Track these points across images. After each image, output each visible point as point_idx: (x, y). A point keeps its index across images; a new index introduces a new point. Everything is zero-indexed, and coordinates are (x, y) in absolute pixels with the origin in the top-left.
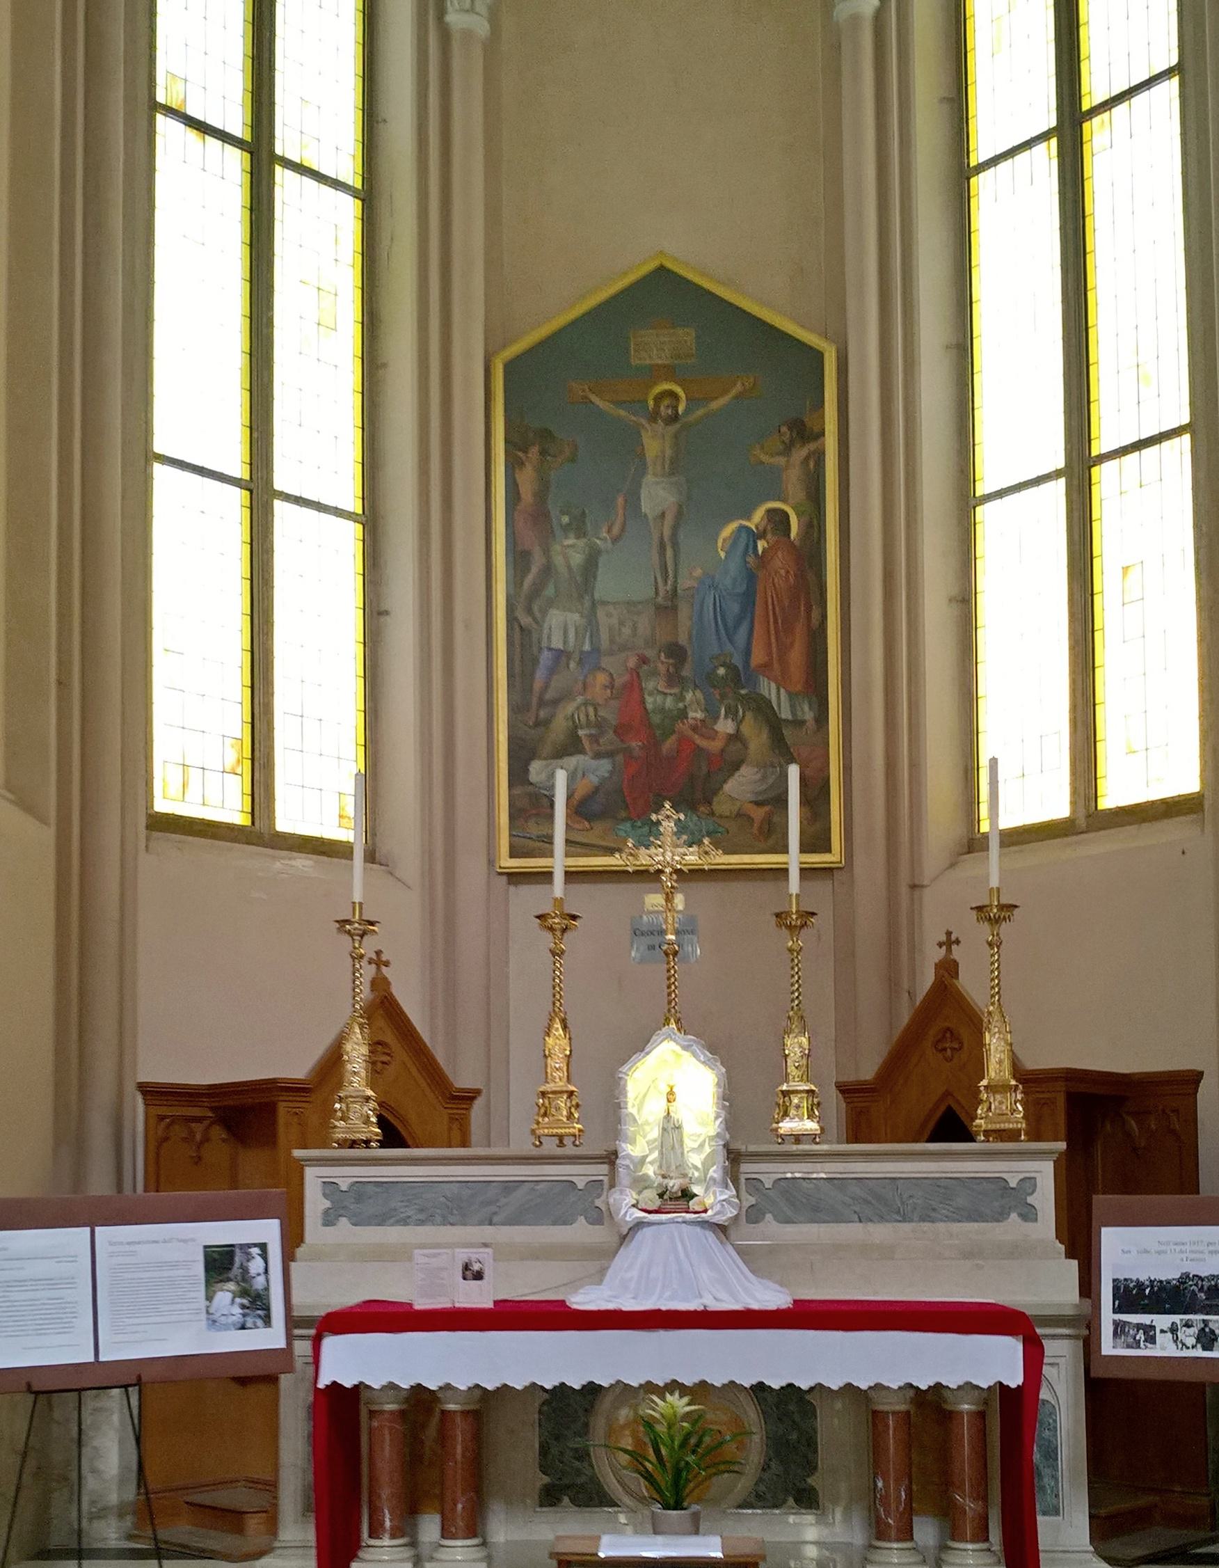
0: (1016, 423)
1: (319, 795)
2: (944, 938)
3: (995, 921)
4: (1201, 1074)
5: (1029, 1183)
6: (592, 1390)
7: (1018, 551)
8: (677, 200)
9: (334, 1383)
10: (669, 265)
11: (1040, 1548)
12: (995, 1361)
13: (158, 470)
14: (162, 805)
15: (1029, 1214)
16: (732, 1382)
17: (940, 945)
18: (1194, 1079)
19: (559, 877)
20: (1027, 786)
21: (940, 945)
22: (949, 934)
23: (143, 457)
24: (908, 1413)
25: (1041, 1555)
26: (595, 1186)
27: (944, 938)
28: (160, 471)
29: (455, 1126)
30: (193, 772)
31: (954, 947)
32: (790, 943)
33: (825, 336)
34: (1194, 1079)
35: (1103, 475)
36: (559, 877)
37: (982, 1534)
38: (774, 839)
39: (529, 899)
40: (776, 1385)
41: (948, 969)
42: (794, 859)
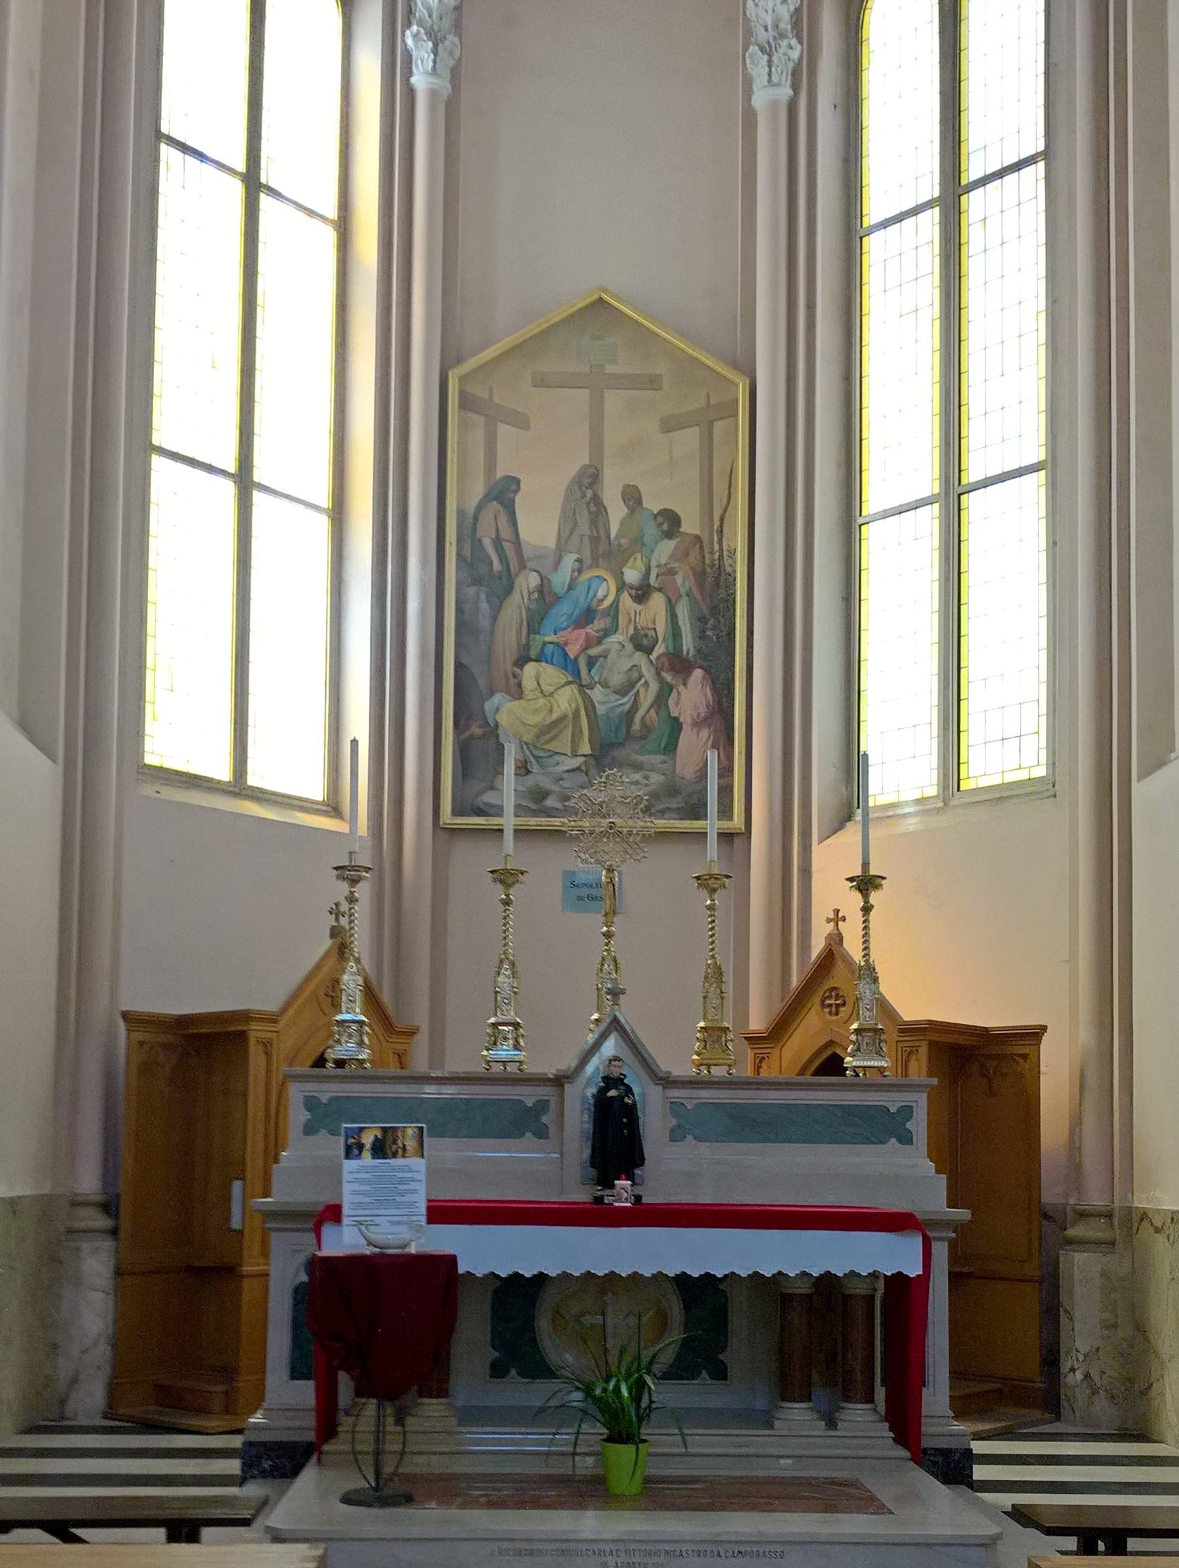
0: (897, 454)
1: (290, 762)
2: (832, 916)
3: (508, 886)
4: (1044, 1028)
5: (907, 1112)
6: (541, 1278)
7: (896, 566)
8: (602, 222)
9: (684, 1273)
10: (605, 297)
11: (923, 1413)
12: (899, 1255)
13: (157, 461)
14: (149, 759)
15: (906, 1139)
16: (853, 1271)
17: (829, 920)
18: (1034, 1035)
19: (509, 835)
20: (900, 770)
21: (829, 920)
22: (837, 911)
23: (144, 448)
24: (809, 1296)
25: (923, 1420)
26: (542, 1106)
27: (832, 916)
28: (158, 463)
29: (1133, 1544)
30: (181, 730)
31: (840, 923)
32: (708, 902)
33: (736, 366)
34: (1034, 1035)
35: (972, 502)
36: (509, 835)
37: (869, 1399)
38: (697, 810)
39: (486, 858)
40: (744, 1274)
41: (836, 939)
42: (712, 825)
